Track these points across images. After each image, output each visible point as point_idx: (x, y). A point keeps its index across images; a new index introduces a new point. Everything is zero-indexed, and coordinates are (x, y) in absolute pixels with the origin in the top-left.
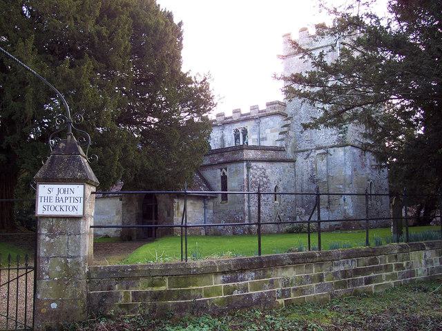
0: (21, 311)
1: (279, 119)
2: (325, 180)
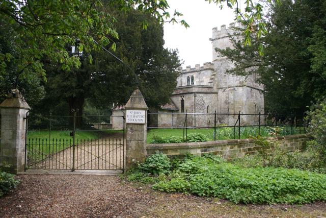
0: (118, 161)
1: (210, 72)
2: (232, 103)
